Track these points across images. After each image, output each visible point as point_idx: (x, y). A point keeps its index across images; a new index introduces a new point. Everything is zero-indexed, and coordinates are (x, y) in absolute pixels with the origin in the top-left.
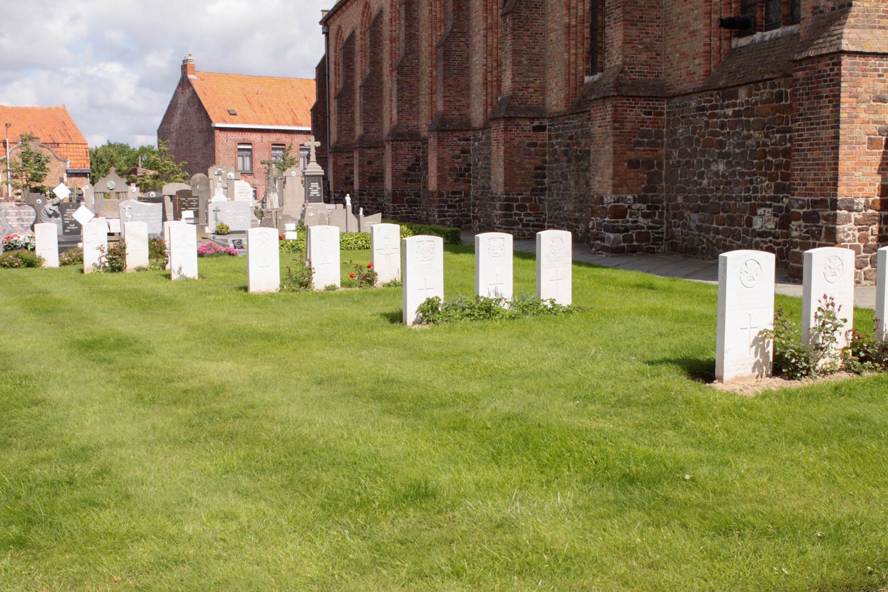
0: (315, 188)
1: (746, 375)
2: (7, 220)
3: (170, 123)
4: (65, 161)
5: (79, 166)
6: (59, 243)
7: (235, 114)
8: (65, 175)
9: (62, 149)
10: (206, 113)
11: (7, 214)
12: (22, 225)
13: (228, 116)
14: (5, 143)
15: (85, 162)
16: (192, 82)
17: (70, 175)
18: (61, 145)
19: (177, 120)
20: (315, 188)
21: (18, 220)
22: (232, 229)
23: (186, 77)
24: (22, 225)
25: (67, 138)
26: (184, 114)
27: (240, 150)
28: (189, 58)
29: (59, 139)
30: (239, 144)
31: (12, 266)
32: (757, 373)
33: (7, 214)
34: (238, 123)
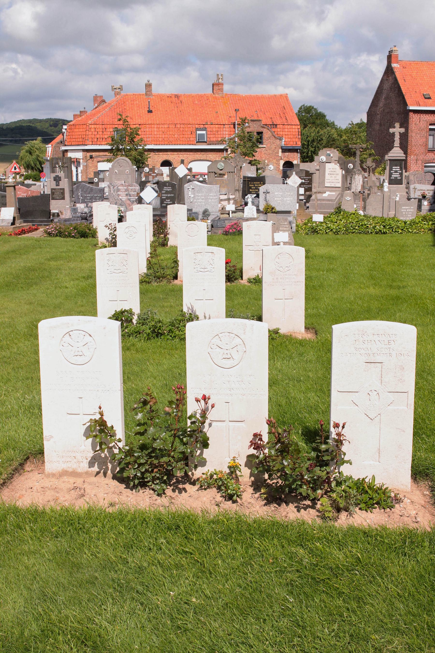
0: (396, 172)
1: (79, 470)
2: (119, 195)
3: (377, 106)
4: (281, 139)
5: (291, 143)
6: (154, 216)
7: (430, 98)
8: (280, 150)
9: (278, 130)
10: (404, 98)
11: (118, 190)
12: (129, 199)
13: (422, 100)
14: (234, 125)
15: (297, 140)
16: (395, 70)
17: (285, 150)
18: (278, 126)
19: (381, 104)
20: (396, 172)
21: (127, 195)
22: (278, 209)
23: (391, 65)
24: (129, 199)
25: (284, 119)
26: (387, 98)
27: (431, 129)
28: (394, 49)
29: (278, 121)
30: (430, 125)
31: (70, 236)
32: (96, 469)
33: (118, 190)
34: (431, 106)
